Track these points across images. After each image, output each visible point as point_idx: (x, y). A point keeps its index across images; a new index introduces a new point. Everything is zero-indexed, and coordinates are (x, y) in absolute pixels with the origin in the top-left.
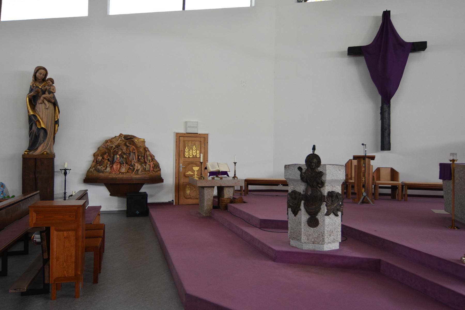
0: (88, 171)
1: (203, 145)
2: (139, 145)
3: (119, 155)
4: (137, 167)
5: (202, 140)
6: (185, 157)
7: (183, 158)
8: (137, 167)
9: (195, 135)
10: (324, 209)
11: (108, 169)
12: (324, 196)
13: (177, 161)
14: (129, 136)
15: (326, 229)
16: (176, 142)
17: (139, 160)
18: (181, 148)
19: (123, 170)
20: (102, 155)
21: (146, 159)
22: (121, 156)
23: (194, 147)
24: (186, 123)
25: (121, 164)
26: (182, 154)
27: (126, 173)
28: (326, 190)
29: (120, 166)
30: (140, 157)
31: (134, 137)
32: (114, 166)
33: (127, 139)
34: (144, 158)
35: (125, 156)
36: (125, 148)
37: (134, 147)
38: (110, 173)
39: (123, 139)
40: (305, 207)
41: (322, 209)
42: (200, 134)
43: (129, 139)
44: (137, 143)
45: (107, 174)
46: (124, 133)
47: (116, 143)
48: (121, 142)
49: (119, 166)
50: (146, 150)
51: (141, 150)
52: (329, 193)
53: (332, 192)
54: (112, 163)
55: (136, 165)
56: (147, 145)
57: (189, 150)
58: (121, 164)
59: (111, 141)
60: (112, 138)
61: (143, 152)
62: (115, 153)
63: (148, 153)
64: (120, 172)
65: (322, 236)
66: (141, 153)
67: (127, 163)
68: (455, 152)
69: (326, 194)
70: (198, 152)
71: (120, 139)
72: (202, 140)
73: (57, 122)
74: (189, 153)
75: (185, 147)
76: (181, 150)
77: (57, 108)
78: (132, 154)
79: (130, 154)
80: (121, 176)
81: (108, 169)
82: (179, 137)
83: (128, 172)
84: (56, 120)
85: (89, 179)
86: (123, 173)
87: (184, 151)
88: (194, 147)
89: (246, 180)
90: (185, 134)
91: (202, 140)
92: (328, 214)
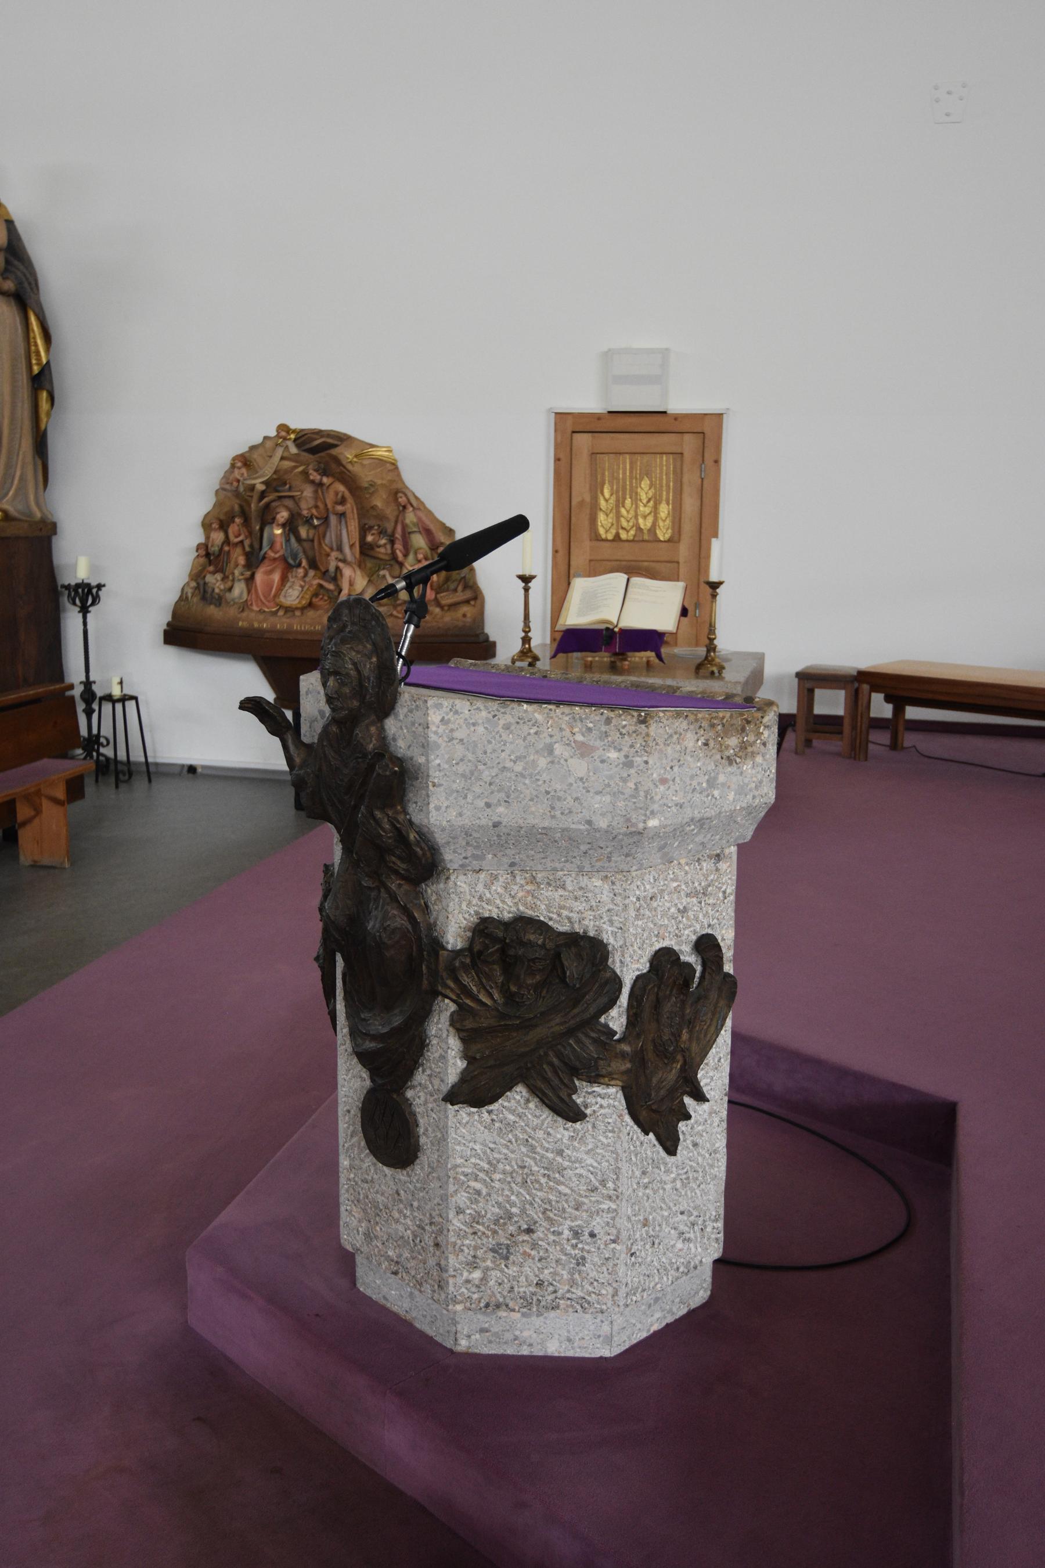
0: (183, 598)
1: (691, 477)
2: (366, 475)
3: (283, 526)
4: (351, 584)
5: (684, 446)
6: (597, 538)
7: (587, 544)
8: (351, 584)
9: (653, 422)
10: (446, 1057)
11: (239, 589)
12: (437, 945)
13: (562, 552)
14: (319, 433)
15: (462, 1198)
16: (557, 459)
17: (366, 550)
18: (581, 490)
19: (293, 595)
20: (223, 526)
21: (398, 546)
22: (290, 527)
23: (645, 483)
24: (607, 356)
25: (288, 566)
26: (581, 521)
27: (303, 609)
28: (459, 907)
29: (284, 579)
30: (370, 538)
31: (343, 439)
32: (259, 577)
33: (313, 451)
34: (392, 542)
35: (303, 532)
36: (308, 492)
37: (341, 488)
38: (245, 606)
39: (294, 450)
40: (345, 998)
41: (433, 1053)
42: (676, 417)
43: (320, 449)
44: (356, 469)
45: (233, 612)
46: (303, 421)
47: (267, 472)
48: (287, 464)
49: (276, 577)
50: (401, 498)
51: (378, 502)
52: (484, 929)
53: (523, 923)
54: (254, 560)
55: (347, 572)
56: (414, 480)
57: (620, 503)
58: (288, 566)
59: (245, 461)
60: (253, 448)
61: (390, 512)
62: (267, 517)
63: (410, 517)
64: (281, 607)
65: (437, 1245)
66: (381, 517)
67: (313, 564)
68: (322, 868)
69: (454, 933)
70: (664, 510)
71: (280, 452)
72: (684, 446)
73: (41, 381)
74: (618, 516)
75: (596, 488)
76: (582, 503)
77: (33, 319)
78: (333, 520)
79: (326, 520)
80: (281, 623)
81: (239, 589)
82: (571, 428)
83: (310, 605)
84: (36, 369)
85: (185, 633)
86: (289, 610)
87: (595, 508)
88: (645, 483)
89: (803, 677)
90: (598, 417)
91: (689, 444)
92: (475, 1091)
